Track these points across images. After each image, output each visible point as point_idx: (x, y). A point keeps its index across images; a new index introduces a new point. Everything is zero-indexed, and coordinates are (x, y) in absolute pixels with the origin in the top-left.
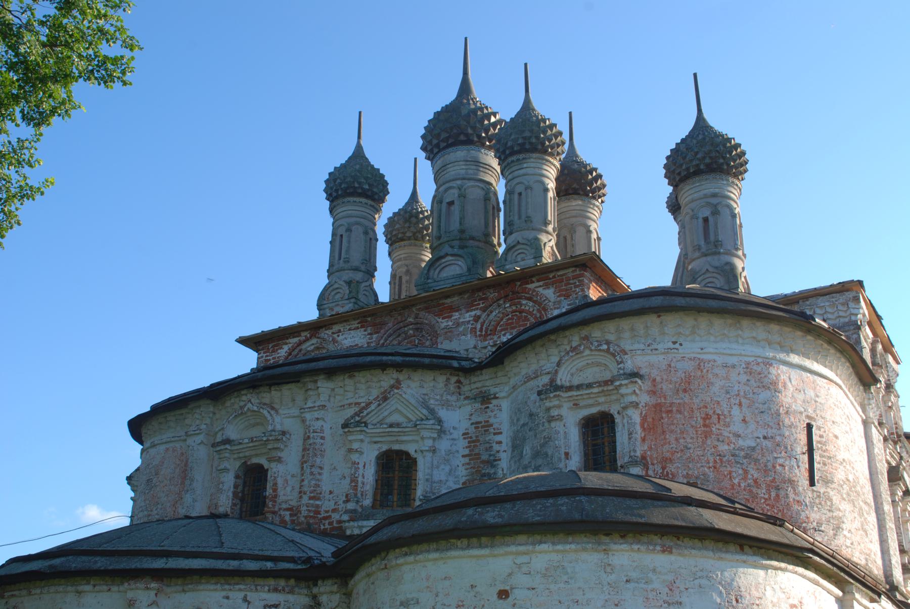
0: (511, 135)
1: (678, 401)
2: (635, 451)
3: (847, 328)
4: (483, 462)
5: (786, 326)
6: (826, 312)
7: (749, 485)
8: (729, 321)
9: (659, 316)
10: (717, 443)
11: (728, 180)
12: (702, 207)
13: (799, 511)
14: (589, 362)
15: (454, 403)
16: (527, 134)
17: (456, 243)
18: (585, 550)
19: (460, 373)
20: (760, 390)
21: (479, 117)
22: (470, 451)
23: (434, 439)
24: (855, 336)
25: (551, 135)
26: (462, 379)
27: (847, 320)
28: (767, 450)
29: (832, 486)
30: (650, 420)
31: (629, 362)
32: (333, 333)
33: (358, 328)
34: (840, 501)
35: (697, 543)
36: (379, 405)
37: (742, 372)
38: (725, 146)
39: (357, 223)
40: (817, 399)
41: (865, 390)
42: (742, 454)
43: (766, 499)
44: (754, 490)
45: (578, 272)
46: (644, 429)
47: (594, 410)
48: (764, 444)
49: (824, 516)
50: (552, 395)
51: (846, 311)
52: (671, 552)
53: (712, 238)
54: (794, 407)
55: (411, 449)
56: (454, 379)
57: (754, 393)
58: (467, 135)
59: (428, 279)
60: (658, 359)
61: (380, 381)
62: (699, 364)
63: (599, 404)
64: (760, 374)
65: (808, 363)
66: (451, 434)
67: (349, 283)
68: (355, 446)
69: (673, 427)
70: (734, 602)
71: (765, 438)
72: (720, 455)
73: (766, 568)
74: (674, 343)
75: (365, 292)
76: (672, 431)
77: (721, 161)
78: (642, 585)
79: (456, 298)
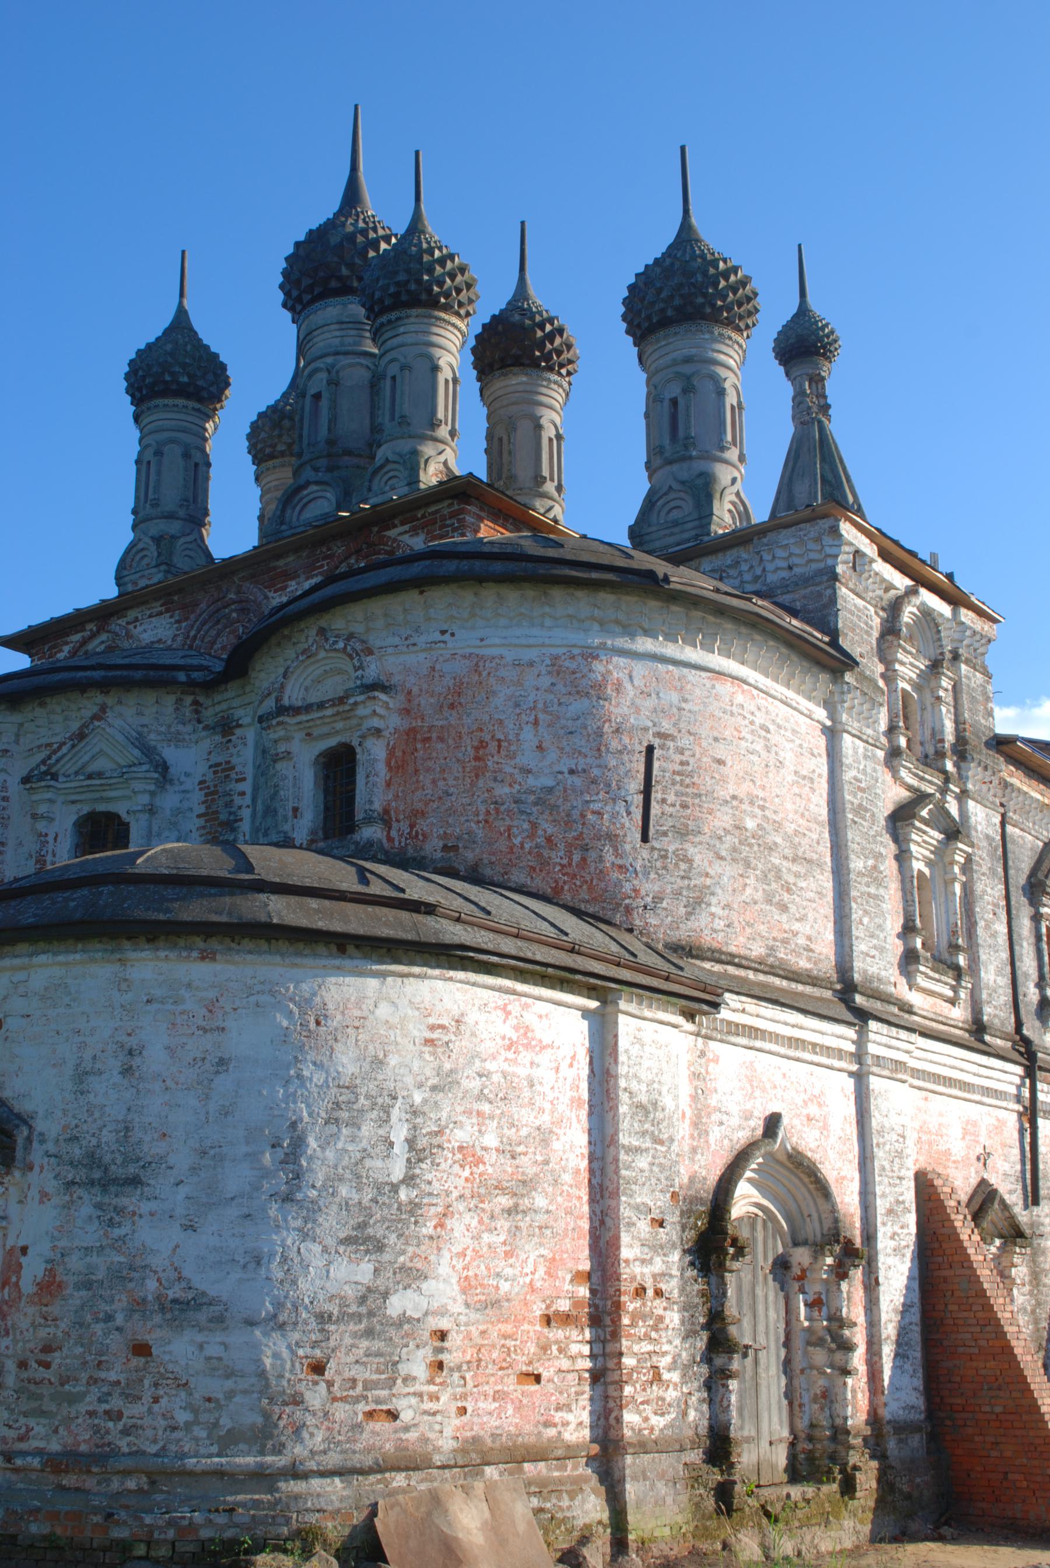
0: (378, 280)
1: (441, 723)
2: (371, 802)
3: (817, 580)
4: (222, 824)
5: (628, 594)
6: (791, 555)
7: (537, 846)
8: (530, 593)
9: (422, 592)
10: (493, 785)
11: (712, 333)
12: (669, 381)
13: (620, 881)
14: (327, 668)
15: (187, 737)
16: (402, 277)
17: (323, 462)
18: (93, 960)
19: (197, 690)
20: (572, 699)
21: (359, 246)
22: (207, 808)
23: (153, 794)
24: (829, 592)
25: (443, 275)
26: (201, 699)
27: (822, 565)
28: (574, 791)
29: (697, 840)
30: (399, 754)
31: (373, 666)
32: (128, 623)
33: (160, 614)
34: (710, 862)
35: (263, 945)
36: (73, 746)
37: (544, 672)
38: (705, 273)
39: (172, 441)
40: (684, 705)
41: (835, 681)
42: (532, 798)
43: (563, 866)
44: (546, 853)
45: (456, 507)
46: (390, 768)
47: (332, 742)
48: (569, 782)
49: (669, 886)
50: (274, 722)
51: (820, 551)
52: (214, 959)
53: (681, 434)
54: (632, 720)
55: (121, 809)
56: (189, 700)
57: (560, 704)
58: (340, 278)
59: (282, 523)
60: (417, 660)
61: (79, 709)
62: (477, 665)
63: (337, 732)
64: (574, 673)
65: (671, 650)
66: (181, 783)
67: (158, 540)
68: (42, 809)
69: (430, 764)
70: (312, 1025)
71: (572, 772)
72: (496, 803)
73: (383, 975)
74: (443, 632)
75: (187, 552)
76: (428, 770)
77: (700, 300)
78: (169, 1007)
79: (291, 559)
